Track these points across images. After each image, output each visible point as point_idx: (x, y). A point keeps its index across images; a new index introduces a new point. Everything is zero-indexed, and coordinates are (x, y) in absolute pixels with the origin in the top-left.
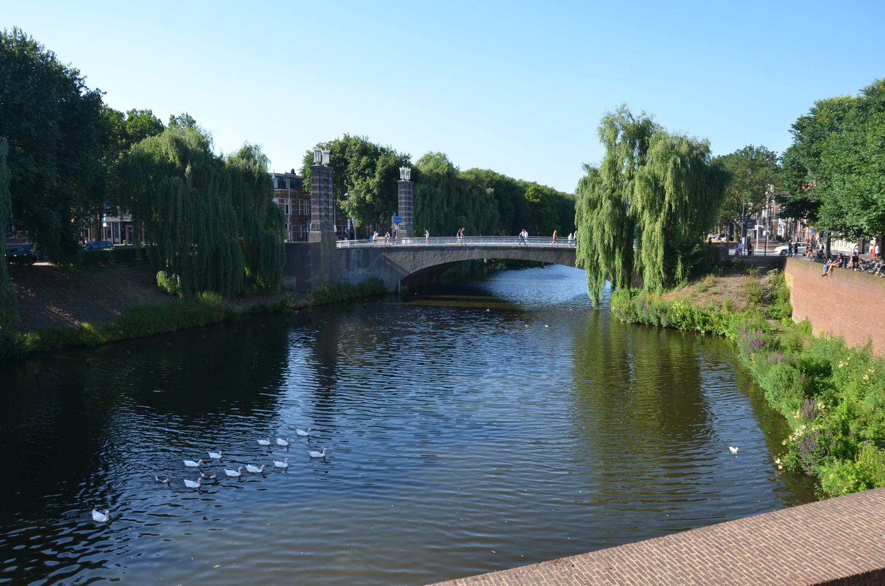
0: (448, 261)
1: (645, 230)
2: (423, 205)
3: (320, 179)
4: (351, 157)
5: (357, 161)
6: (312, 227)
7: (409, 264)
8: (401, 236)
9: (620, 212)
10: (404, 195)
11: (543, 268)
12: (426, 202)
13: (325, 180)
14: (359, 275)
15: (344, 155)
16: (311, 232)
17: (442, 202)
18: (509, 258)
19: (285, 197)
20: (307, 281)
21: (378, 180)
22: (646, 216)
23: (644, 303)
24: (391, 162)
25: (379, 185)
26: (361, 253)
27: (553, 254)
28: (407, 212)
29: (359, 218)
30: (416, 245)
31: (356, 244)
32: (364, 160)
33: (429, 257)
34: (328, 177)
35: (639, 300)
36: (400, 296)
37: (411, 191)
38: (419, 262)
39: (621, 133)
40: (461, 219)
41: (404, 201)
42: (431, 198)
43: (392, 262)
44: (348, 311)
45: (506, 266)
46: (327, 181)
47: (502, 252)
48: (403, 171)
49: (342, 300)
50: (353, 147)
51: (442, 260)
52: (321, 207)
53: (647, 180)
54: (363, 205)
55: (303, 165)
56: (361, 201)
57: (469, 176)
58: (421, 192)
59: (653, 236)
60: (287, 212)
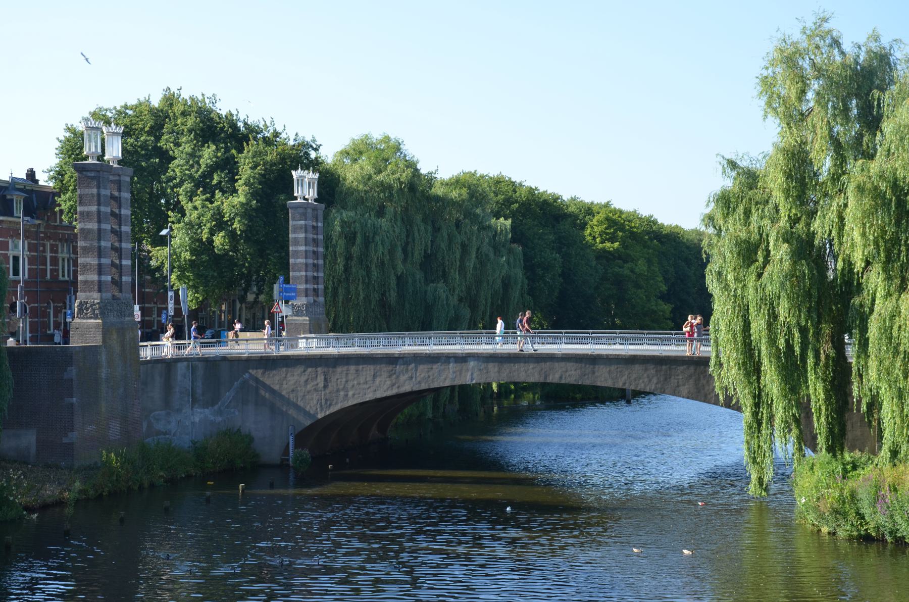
0: (407, 388)
1: (875, 313)
2: (348, 258)
3: (99, 195)
4: (178, 145)
5: (192, 155)
6: (80, 310)
7: (315, 396)
8: (296, 330)
9: (811, 270)
10: (302, 235)
11: (629, 402)
12: (355, 250)
13: (113, 197)
14: (193, 423)
15: (158, 139)
16: (77, 320)
17: (392, 252)
18: (549, 380)
19: (12, 237)
20: (65, 440)
21: (242, 199)
22: (875, 280)
23: (878, 488)
24: (271, 156)
25: (246, 212)
26: (200, 372)
27: (653, 372)
28: (311, 248)
29: (195, 288)
30: (332, 351)
31: (192, 348)
32: (208, 154)
33: (362, 380)
34: (120, 190)
35: (865, 480)
36: (291, 475)
37: (320, 224)
38: (338, 391)
39: (815, 85)
40: (435, 291)
41: (303, 248)
42: (367, 242)
43: (273, 391)
44: (166, 510)
45: (541, 398)
46: (117, 200)
47: (531, 366)
48: (301, 179)
49: (152, 486)
50: (179, 121)
51: (393, 385)
52: (103, 261)
53: (877, 193)
54: (205, 257)
55: (57, 161)
56: (202, 248)
57: (454, 194)
58: (342, 227)
59: (895, 328)
60: (16, 273)
